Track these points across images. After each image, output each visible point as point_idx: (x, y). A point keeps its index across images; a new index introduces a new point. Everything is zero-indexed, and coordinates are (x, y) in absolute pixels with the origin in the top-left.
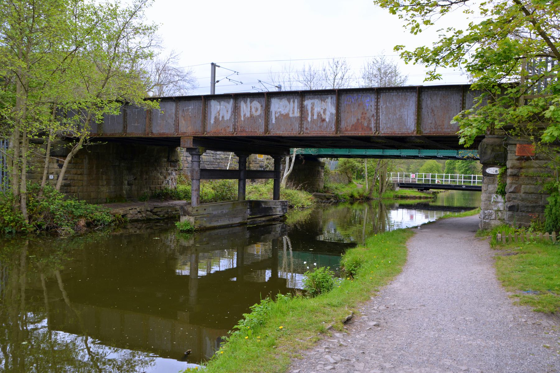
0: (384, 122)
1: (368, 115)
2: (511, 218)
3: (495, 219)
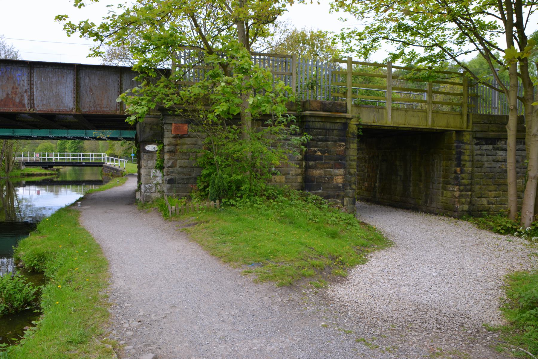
0: (40, 98)
1: (20, 90)
2: (170, 189)
3: (155, 192)
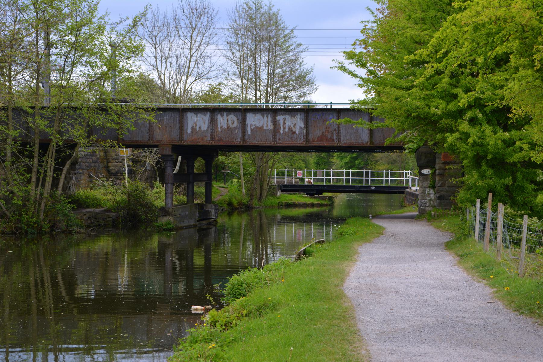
0: (344, 135)
1: (331, 129)
2: (439, 204)
3: (429, 206)
